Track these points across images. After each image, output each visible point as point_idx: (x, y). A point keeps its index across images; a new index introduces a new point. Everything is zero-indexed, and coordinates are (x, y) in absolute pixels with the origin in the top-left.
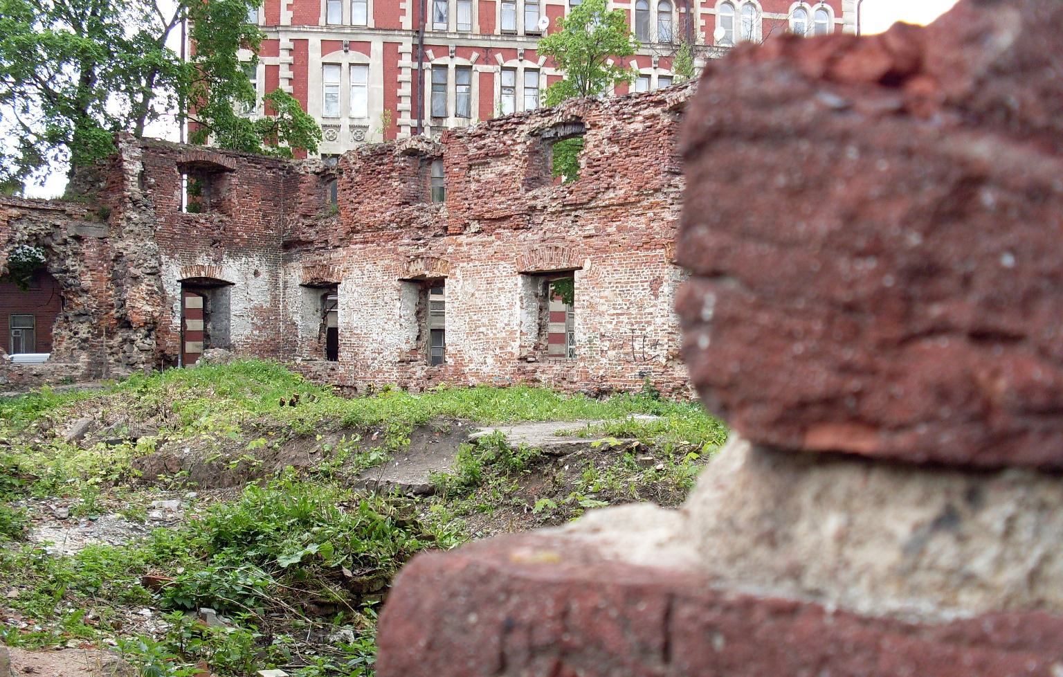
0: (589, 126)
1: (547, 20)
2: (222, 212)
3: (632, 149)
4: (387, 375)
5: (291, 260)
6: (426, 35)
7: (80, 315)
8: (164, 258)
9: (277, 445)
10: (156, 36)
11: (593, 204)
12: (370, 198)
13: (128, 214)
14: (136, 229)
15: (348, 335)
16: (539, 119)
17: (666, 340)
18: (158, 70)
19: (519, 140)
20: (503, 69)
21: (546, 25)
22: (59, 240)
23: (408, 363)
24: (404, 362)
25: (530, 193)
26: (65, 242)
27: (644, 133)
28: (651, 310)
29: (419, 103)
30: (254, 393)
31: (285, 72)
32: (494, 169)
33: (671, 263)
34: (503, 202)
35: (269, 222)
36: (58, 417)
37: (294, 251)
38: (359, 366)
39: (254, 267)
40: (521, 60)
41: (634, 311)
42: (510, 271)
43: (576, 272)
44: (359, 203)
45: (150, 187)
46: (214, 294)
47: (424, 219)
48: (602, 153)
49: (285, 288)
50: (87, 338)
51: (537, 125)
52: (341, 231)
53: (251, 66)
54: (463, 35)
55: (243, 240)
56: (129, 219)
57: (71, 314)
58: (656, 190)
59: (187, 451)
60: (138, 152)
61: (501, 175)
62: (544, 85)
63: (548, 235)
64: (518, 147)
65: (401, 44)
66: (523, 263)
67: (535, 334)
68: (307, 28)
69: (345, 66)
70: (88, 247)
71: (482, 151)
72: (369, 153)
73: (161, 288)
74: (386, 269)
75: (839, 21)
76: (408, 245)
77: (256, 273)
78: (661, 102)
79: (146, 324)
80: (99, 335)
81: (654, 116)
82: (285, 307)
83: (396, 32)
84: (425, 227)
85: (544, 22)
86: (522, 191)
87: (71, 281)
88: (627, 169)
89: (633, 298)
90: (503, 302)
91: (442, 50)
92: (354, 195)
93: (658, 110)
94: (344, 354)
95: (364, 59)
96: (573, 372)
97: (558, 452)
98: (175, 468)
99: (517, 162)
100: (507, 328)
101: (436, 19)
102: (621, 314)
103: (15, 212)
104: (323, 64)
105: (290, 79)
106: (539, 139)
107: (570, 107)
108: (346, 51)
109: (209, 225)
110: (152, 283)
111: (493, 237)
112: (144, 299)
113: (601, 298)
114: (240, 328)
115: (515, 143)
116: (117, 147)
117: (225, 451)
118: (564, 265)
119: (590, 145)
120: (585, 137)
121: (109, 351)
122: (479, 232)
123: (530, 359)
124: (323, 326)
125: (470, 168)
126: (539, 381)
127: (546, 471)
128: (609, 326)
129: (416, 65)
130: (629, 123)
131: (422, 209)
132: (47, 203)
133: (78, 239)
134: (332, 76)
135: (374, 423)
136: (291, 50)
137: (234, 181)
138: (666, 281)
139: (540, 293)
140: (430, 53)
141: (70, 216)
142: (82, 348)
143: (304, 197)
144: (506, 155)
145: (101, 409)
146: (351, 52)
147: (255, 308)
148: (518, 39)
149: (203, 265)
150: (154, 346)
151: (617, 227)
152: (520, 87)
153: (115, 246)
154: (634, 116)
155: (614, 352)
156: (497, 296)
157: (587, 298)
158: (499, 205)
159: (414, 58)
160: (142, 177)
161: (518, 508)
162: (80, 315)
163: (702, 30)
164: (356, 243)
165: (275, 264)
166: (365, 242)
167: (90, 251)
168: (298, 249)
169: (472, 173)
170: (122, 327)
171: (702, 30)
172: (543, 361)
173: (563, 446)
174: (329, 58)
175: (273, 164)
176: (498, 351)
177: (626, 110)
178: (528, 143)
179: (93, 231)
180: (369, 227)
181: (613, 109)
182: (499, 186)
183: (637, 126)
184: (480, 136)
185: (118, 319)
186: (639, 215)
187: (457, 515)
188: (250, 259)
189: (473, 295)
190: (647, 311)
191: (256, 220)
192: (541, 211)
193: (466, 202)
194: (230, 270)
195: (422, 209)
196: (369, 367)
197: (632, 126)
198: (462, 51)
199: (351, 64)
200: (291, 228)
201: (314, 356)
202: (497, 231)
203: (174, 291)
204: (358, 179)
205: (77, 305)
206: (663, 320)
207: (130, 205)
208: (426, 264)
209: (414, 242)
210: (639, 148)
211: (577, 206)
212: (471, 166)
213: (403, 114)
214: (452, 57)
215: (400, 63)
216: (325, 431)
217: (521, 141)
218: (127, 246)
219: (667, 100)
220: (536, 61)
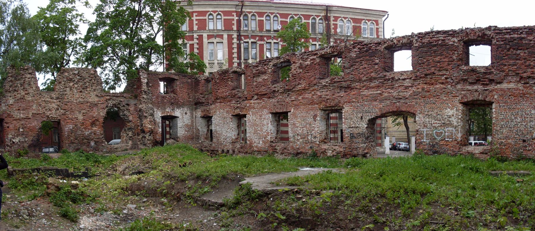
0: (292, 63)
1: (281, 26)
2: (174, 94)
3: (307, 70)
4: (228, 147)
5: (197, 109)
6: (241, 32)
7: (129, 129)
8: (155, 110)
9: (174, 184)
10: (152, 37)
11: (294, 90)
12: (222, 88)
13: (143, 96)
14: (146, 101)
15: (215, 133)
16: (276, 60)
17: (319, 136)
18: (156, 49)
19: (269, 68)
20: (267, 43)
21: (280, 28)
22: (122, 105)
23: (235, 143)
24: (233, 143)
25: (273, 86)
26: (124, 106)
27: (310, 65)
28: (314, 125)
29: (240, 55)
30: (181, 155)
31: (196, 46)
33: (320, 109)
34: (264, 89)
35: (190, 96)
36: (118, 164)
37: (198, 105)
38: (219, 144)
39: (185, 111)
40: (272, 40)
41: (308, 126)
43: (289, 113)
44: (218, 89)
45: (150, 87)
46: (172, 120)
47: (239, 95)
48: (297, 72)
49: (196, 118)
50: (131, 136)
51: (275, 62)
52: (213, 99)
53: (185, 45)
54: (253, 31)
55: (181, 102)
56: (143, 97)
57: (126, 129)
58: (315, 85)
59: (146, 183)
60: (146, 76)
61: (264, 79)
62: (280, 48)
63: (280, 100)
64: (269, 70)
65: (233, 35)
66: (271, 109)
67: (275, 133)
68: (202, 31)
69: (215, 43)
70: (131, 107)
71: (258, 72)
72: (221, 73)
73: (154, 120)
74: (227, 112)
75: (378, 27)
76: (234, 103)
77: (186, 113)
78: (316, 54)
79: (149, 131)
80: (135, 135)
81: (313, 59)
82: (196, 124)
83: (231, 31)
84: (240, 97)
85: (280, 27)
86: (271, 85)
87: (126, 118)
88: (305, 77)
89: (307, 122)
90: (265, 122)
91: (246, 37)
92: (217, 87)
93: (315, 57)
94: (214, 140)
95: (221, 41)
96: (288, 147)
97: (269, 193)
98: (142, 189)
99: (269, 75)
100: (266, 132)
101: (244, 26)
102: (304, 127)
103: (108, 97)
104: (208, 43)
105: (197, 48)
106: (276, 67)
107: (286, 56)
108: (215, 38)
109: (170, 98)
110: (151, 118)
111: (262, 101)
112: (148, 123)
113: (297, 121)
114: (181, 132)
115: (268, 69)
116: (139, 74)
117: (158, 184)
118: (285, 110)
119: (293, 69)
120: (291, 66)
121: (138, 140)
122: (257, 99)
123: (274, 142)
124: (208, 130)
125: (254, 77)
126: (277, 149)
127: (264, 200)
128: (300, 131)
130: (306, 62)
131: (238, 91)
132: (118, 94)
133: (128, 105)
134: (211, 47)
135: (207, 176)
136: (197, 38)
138: (318, 116)
139: (277, 119)
140: (243, 38)
141: (125, 97)
142: (130, 139)
143: (201, 88)
144: (264, 73)
145: (132, 161)
146: (217, 38)
147: (186, 125)
148: (271, 33)
149: (168, 111)
150: (152, 138)
151: (302, 97)
152: (272, 49)
153: (139, 106)
154: (307, 59)
155: (302, 140)
157: (292, 122)
158: (263, 90)
160: (147, 83)
161: (253, 215)
163: (333, 29)
164: (218, 103)
165: (192, 110)
166: (221, 102)
167: (132, 108)
168: (200, 105)
169: (255, 79)
170: (142, 132)
171: (333, 29)
172: (278, 143)
173: (270, 190)
174: (210, 41)
175: (191, 76)
177: (304, 57)
178: (272, 69)
179: (132, 102)
180: (222, 97)
181: (300, 57)
183: (308, 63)
184: (257, 66)
185: (141, 130)
186: (309, 93)
187: (231, 216)
188: (184, 109)
189: (255, 120)
190: (312, 126)
191: (186, 96)
192: (277, 92)
193: (253, 89)
194: (177, 113)
195: (238, 91)
196: (222, 144)
197: (306, 63)
198: (253, 37)
199: (217, 42)
200: (197, 98)
201: (205, 140)
202: (263, 99)
203: (159, 120)
204: (218, 81)
205: (128, 126)
206: (317, 129)
207: (144, 93)
208: (240, 110)
209: (236, 102)
210: (309, 70)
211: (289, 90)
212: (254, 76)
213: (234, 58)
214: (250, 39)
215: (233, 41)
216: (190, 179)
217: (270, 68)
218: (143, 106)
219: (318, 53)
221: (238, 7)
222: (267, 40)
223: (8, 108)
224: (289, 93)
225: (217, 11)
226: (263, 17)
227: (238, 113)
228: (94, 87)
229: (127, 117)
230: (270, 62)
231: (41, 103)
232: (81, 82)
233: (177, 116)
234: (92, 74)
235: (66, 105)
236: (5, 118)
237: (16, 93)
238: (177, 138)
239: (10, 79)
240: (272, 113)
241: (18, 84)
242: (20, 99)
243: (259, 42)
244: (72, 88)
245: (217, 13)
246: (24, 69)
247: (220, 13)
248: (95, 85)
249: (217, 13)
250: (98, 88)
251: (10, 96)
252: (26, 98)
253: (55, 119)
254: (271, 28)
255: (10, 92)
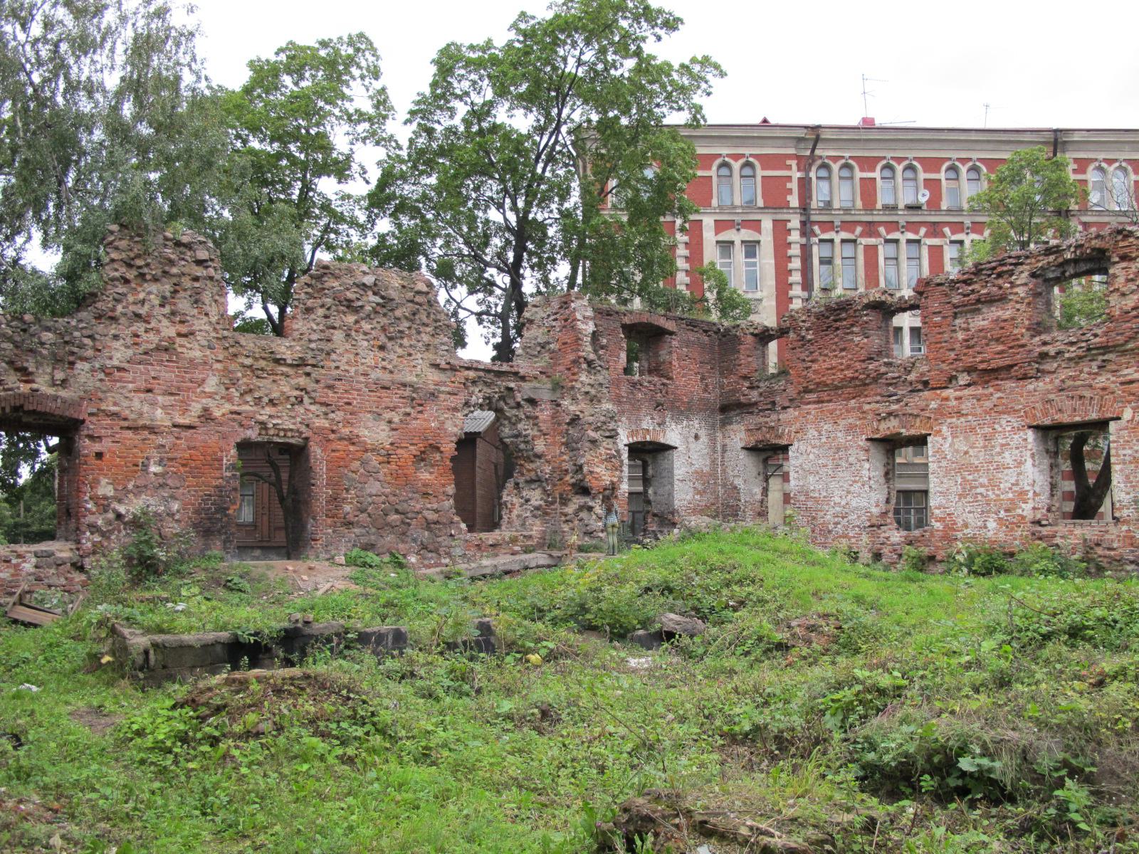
2: (662, 376)
5: (731, 423)
7: (531, 481)
15: (803, 498)
19: (1018, 282)
20: (887, 241)
21: (926, 198)
23: (879, 527)
26: (518, 405)
32: (986, 316)
37: (733, 413)
39: (694, 431)
42: (1015, 425)
44: (812, 361)
46: (655, 458)
51: (1040, 265)
52: (791, 391)
54: (847, 211)
57: (521, 480)
66: (1034, 416)
67: (1047, 493)
70: (542, 410)
74: (850, 429)
77: (697, 437)
80: (553, 503)
82: (724, 471)
86: (1027, 338)
90: (1008, 458)
100: (1015, 488)
115: (1013, 285)
118: (1094, 416)
122: (969, 385)
125: (955, 316)
129: (804, 241)
131: (886, 364)
137: (675, 343)
139: (1052, 448)
140: (816, 228)
142: (535, 516)
144: (1002, 299)
147: (696, 472)
156: (999, 454)
157: (1129, 452)
159: (803, 234)
162: (531, 481)
164: (809, 403)
167: (544, 413)
169: (957, 322)
170: (577, 493)
174: (725, 236)
176: (1002, 513)
178: (1031, 286)
180: (827, 385)
182: (997, 333)
184: (966, 282)
185: (573, 485)
194: (672, 435)
196: (830, 532)
198: (848, 226)
205: (529, 471)
207: (584, 366)
208: (901, 421)
215: (790, 239)
220: (917, 232)
221: (802, 145)
222: (888, 233)
223: (101, 380)
224: (1105, 357)
225: (743, 156)
226: (873, 170)
227: (894, 431)
228: (426, 338)
229: (527, 442)
230: (1022, 264)
231: (240, 375)
232: (385, 315)
233: (672, 444)
234: (419, 293)
235: (330, 387)
236: (88, 419)
237: (139, 327)
238: (672, 513)
239: (116, 270)
240: (1036, 428)
241: (149, 293)
242: (158, 349)
243: (865, 241)
244: (353, 333)
245: (742, 161)
246: (178, 244)
247: (751, 159)
248: (428, 329)
249: (742, 161)
250: (437, 341)
251: (116, 337)
252: (180, 350)
253: (289, 434)
254: (896, 199)
255: (113, 319)
